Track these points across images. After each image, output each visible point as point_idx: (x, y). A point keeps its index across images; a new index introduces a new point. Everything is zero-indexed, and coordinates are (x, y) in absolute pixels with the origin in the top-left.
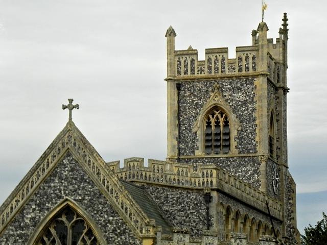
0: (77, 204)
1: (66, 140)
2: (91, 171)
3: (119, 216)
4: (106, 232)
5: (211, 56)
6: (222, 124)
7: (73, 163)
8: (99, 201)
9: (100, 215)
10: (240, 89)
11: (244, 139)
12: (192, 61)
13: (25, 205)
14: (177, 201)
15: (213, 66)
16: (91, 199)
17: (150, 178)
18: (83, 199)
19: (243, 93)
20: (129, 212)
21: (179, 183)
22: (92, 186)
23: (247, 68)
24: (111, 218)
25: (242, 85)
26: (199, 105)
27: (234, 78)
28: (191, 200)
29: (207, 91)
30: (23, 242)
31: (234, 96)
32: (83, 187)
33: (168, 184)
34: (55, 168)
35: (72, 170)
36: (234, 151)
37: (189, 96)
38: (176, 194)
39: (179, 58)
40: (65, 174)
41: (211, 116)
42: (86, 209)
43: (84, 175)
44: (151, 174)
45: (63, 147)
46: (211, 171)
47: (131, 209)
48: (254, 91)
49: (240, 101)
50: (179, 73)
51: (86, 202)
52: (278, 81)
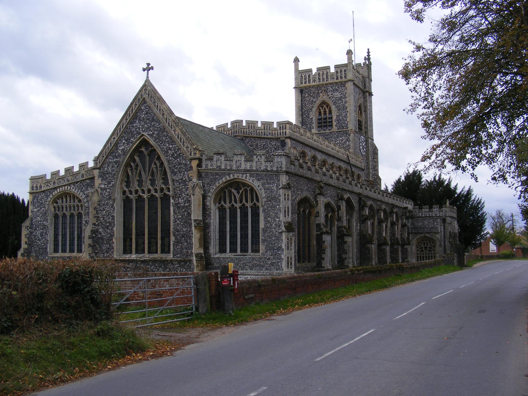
4: (167, 156)
6: (327, 112)
12: (309, 76)
14: (263, 147)
15: (321, 77)
16: (158, 133)
18: (153, 133)
20: (182, 141)
23: (341, 78)
24: (171, 146)
25: (339, 87)
29: (318, 93)
33: (258, 136)
35: (146, 114)
36: (335, 128)
37: (308, 97)
38: (263, 142)
41: (321, 108)
43: (153, 117)
45: (142, 97)
48: (346, 91)
50: (302, 83)
51: (155, 135)
52: (365, 88)
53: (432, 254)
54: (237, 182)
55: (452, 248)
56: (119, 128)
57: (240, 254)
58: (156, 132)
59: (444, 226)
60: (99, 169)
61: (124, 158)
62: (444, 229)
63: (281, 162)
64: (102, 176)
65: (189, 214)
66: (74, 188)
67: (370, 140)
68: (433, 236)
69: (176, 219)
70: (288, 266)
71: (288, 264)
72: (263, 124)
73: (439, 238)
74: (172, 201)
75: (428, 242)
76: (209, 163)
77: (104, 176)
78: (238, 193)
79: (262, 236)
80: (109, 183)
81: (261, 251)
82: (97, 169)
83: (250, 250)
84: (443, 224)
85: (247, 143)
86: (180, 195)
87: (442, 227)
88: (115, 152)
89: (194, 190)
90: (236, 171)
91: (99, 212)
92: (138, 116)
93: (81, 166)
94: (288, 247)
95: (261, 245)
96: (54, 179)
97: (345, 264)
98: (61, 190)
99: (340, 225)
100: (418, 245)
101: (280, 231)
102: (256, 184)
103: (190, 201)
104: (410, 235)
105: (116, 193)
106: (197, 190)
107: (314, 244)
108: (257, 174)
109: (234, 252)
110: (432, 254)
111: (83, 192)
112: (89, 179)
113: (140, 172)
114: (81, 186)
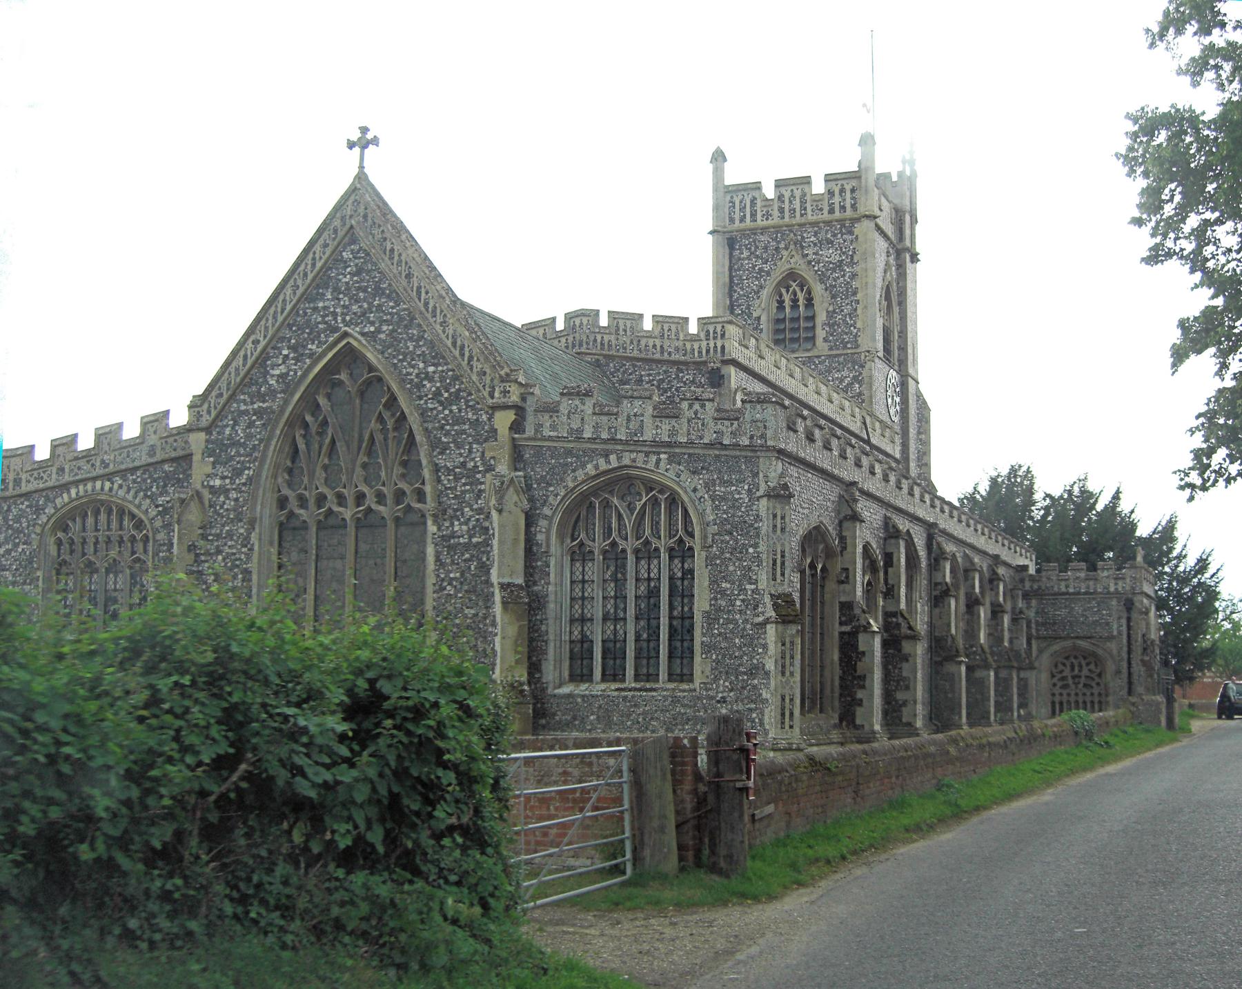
0: (364, 342)
1: (349, 209)
2: (395, 271)
3: (446, 364)
4: (420, 398)
5: (783, 190)
6: (801, 302)
7: (360, 258)
8: (407, 334)
9: (409, 363)
10: (832, 242)
11: (838, 325)
13: (269, 350)
15: (786, 206)
16: (393, 331)
17: (610, 346)
18: (379, 331)
19: (836, 249)
20: (467, 354)
21: (662, 353)
22: (395, 302)
23: (843, 208)
24: (431, 369)
25: (834, 235)
26: (764, 271)
27: (821, 225)
28: (685, 383)
29: (777, 249)
30: (264, 424)
31: (822, 255)
32: (379, 305)
33: (643, 356)
34: (326, 272)
35: (359, 272)
36: (822, 347)
37: (748, 258)
38: (658, 373)
39: (732, 197)
40: (344, 280)
41: (783, 291)
42: (383, 353)
44: (613, 338)
46: (723, 327)
47: (471, 346)
49: (831, 263)
51: (382, 336)
53: (1092, 694)
54: (629, 477)
55: (1149, 680)
56: (272, 311)
57: (633, 685)
58: (385, 328)
59: (1129, 619)
60: (208, 430)
61: (286, 402)
62: (1129, 628)
63: (764, 421)
64: (217, 451)
65: (485, 569)
66: (125, 488)
67: (911, 382)
68: (1098, 646)
69: (443, 580)
70: (783, 723)
71: (783, 715)
72: (657, 322)
73: (1115, 652)
74: (432, 528)
75: (1083, 663)
76: (546, 420)
77: (221, 450)
78: (631, 508)
79: (704, 635)
80: (238, 473)
81: (698, 679)
82: (201, 430)
83: (663, 675)
84: (1125, 615)
85: (612, 373)
86: (456, 510)
87: (1124, 621)
88: (257, 383)
89: (500, 500)
90: (627, 443)
91: (203, 558)
92: (329, 277)
93: (146, 423)
94: (783, 666)
95: (698, 659)
96: (61, 459)
97: (904, 720)
98: (81, 493)
99: (891, 609)
100: (1054, 671)
101: (761, 619)
102: (686, 483)
103: (487, 529)
104: (1033, 642)
105: (259, 502)
106: (511, 497)
107: (833, 660)
108: (690, 455)
109: (615, 680)
110: (1069, 695)
111: (152, 498)
112: (173, 460)
113: (333, 442)
114: (144, 480)
